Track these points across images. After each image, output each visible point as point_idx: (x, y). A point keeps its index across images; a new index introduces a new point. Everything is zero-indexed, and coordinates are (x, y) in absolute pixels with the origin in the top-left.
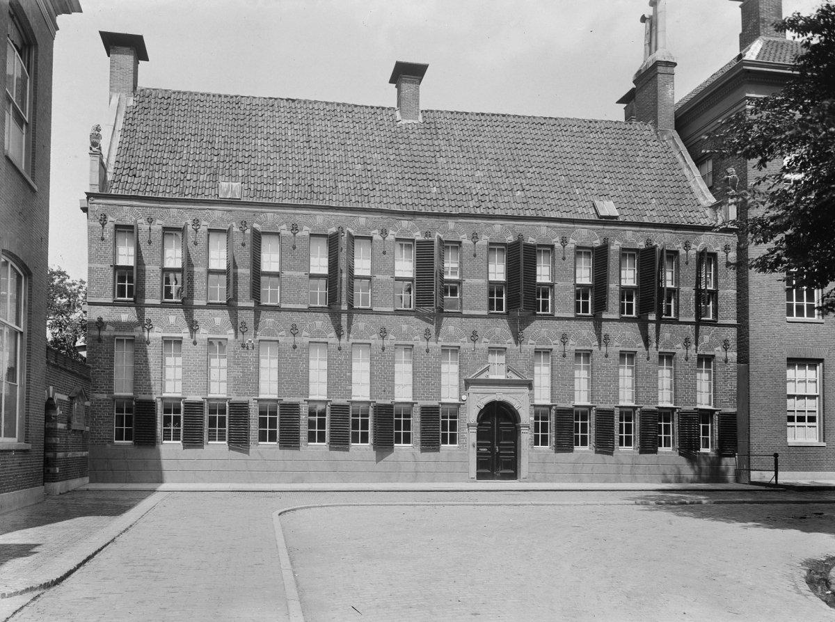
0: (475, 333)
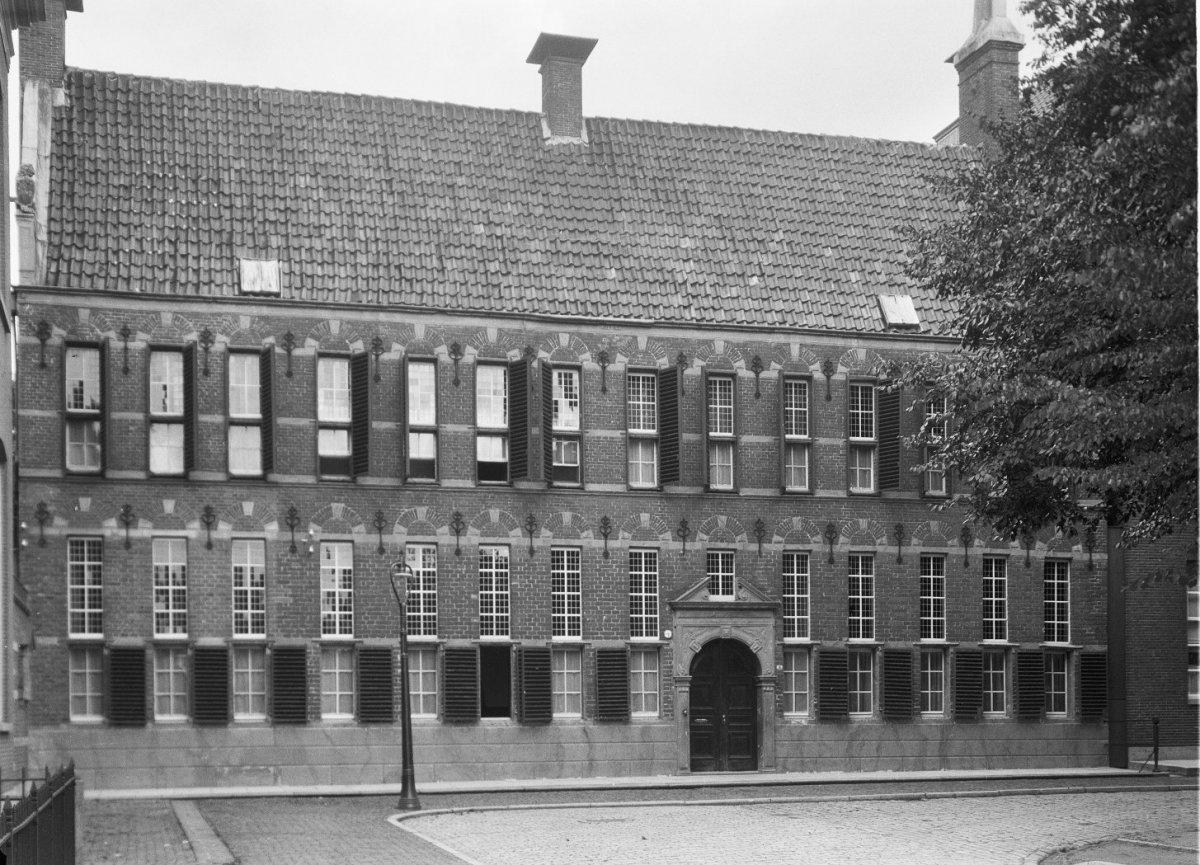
0: (605, 522)
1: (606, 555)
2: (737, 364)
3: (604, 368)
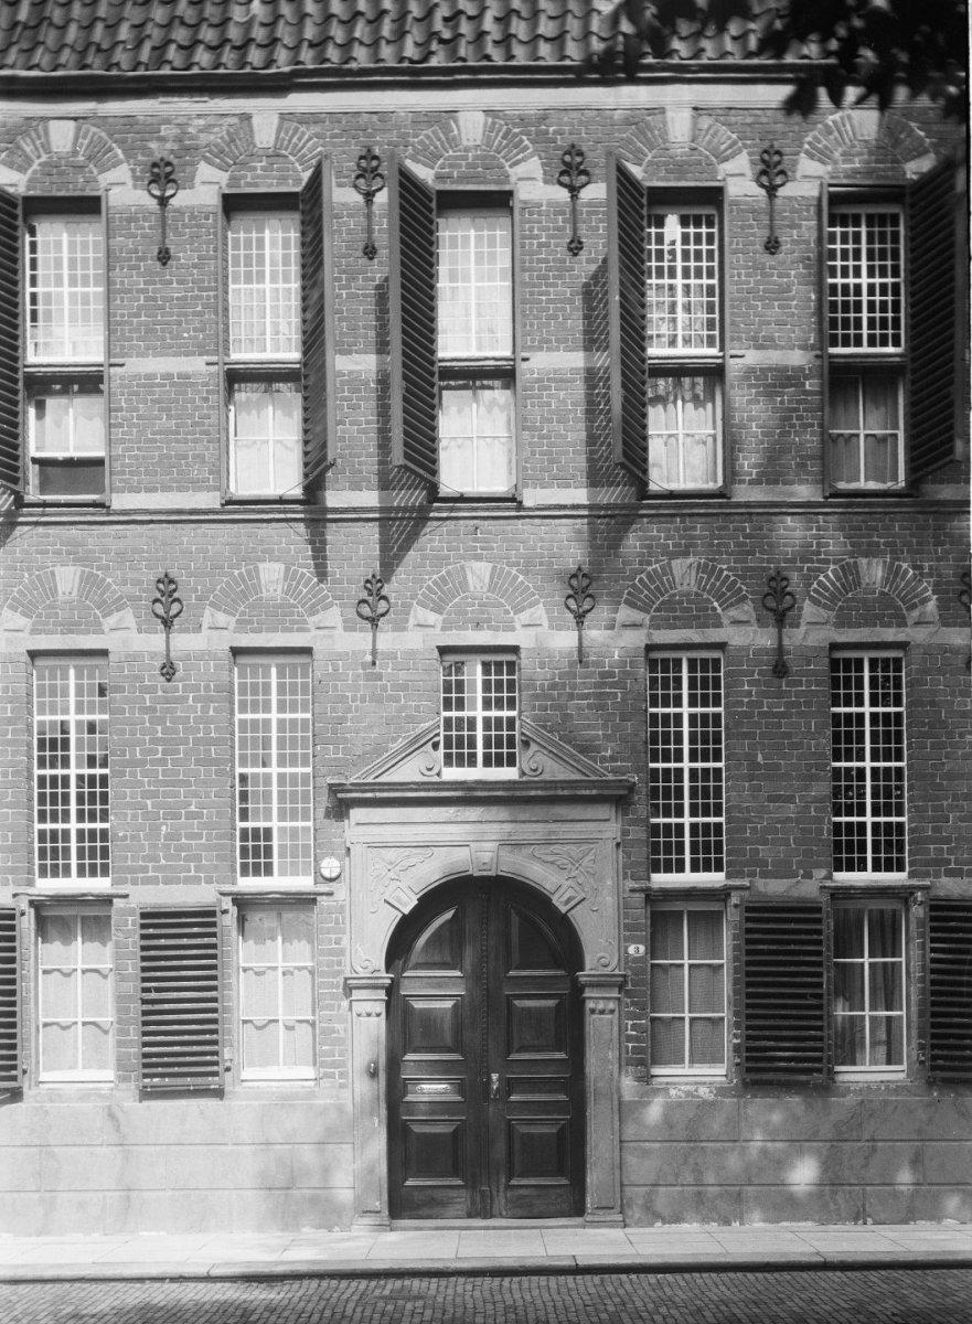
0: (167, 588)
1: (168, 671)
2: (520, 170)
3: (163, 201)
